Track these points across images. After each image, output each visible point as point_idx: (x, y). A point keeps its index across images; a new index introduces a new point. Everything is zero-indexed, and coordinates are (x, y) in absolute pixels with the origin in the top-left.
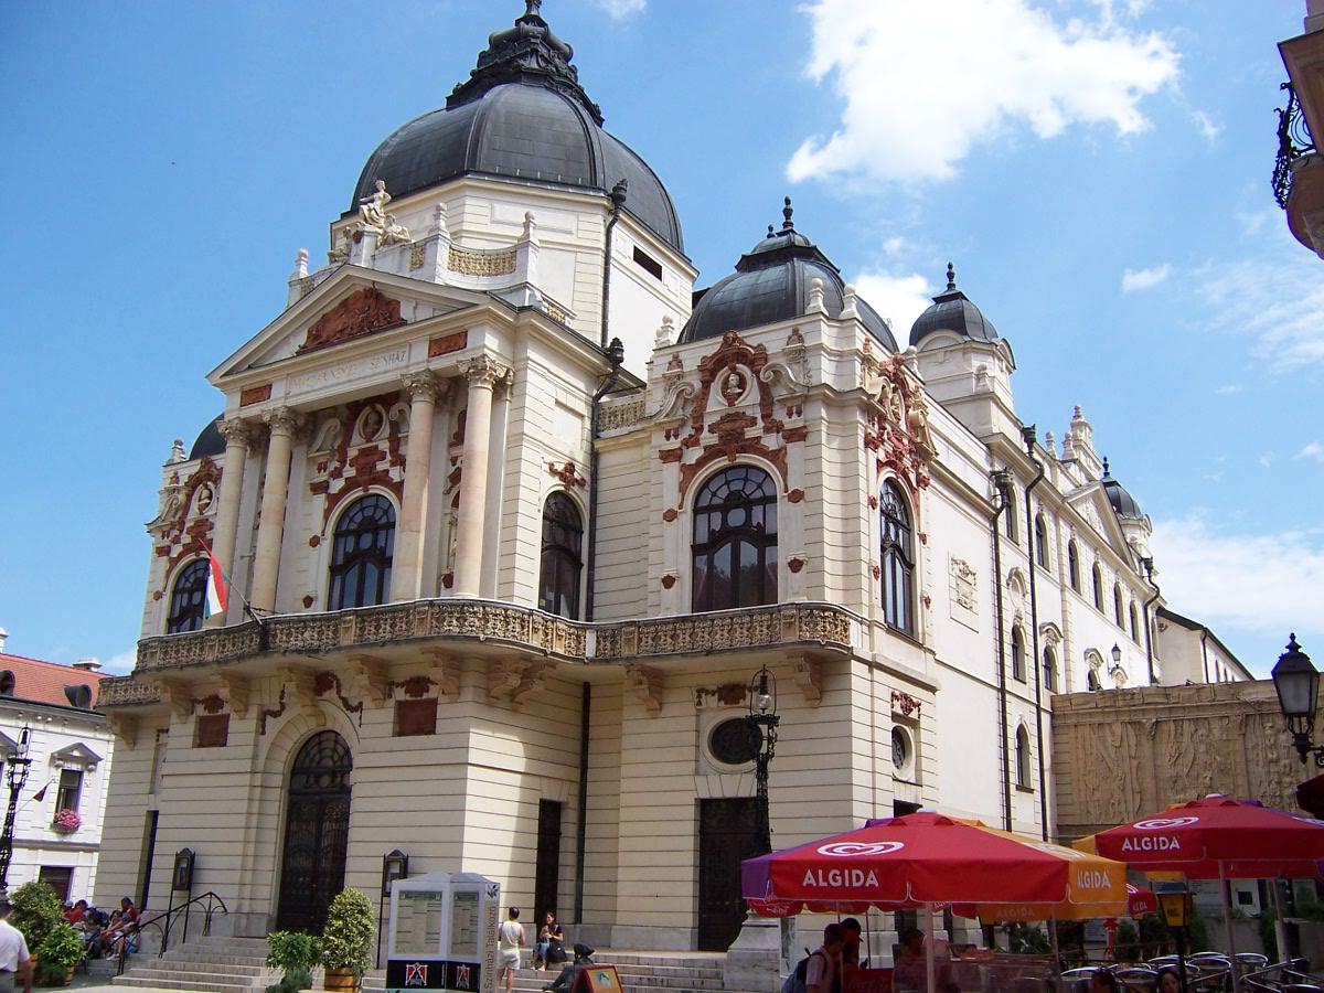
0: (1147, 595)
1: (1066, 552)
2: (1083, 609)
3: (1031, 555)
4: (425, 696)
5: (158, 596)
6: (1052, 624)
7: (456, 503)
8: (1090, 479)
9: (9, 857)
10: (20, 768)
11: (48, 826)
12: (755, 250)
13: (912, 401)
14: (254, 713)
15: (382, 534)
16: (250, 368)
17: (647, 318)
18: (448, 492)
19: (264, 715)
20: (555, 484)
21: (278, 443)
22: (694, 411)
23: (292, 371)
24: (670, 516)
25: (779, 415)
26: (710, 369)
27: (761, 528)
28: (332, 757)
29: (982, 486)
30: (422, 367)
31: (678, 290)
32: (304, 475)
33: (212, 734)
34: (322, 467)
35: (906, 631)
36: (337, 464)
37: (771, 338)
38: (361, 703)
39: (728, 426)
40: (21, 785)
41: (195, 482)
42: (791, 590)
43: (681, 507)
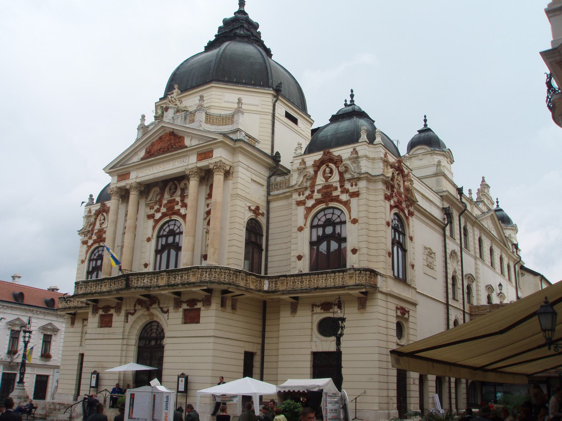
0: (515, 260)
1: (477, 242)
2: (486, 268)
3: (461, 244)
4: (195, 307)
5: (83, 262)
6: (471, 274)
7: (208, 224)
8: (489, 210)
9: (25, 371)
10: (27, 334)
11: (38, 358)
12: (338, 113)
13: (406, 178)
14: (123, 313)
15: (177, 237)
16: (121, 166)
17: (290, 143)
18: (205, 219)
19: (127, 314)
20: (250, 215)
21: (133, 196)
22: (311, 184)
23: (138, 166)
24: (301, 229)
25: (347, 186)
26: (318, 165)
27: (339, 235)
28: (156, 333)
29: (438, 214)
30: (194, 166)
31: (304, 128)
32: (144, 210)
33: (106, 322)
34: (152, 208)
35: (402, 280)
36: (158, 207)
37: (343, 152)
38: (168, 310)
39: (325, 191)
40: (28, 342)
41: (98, 213)
42: (352, 261)
43: (305, 225)
